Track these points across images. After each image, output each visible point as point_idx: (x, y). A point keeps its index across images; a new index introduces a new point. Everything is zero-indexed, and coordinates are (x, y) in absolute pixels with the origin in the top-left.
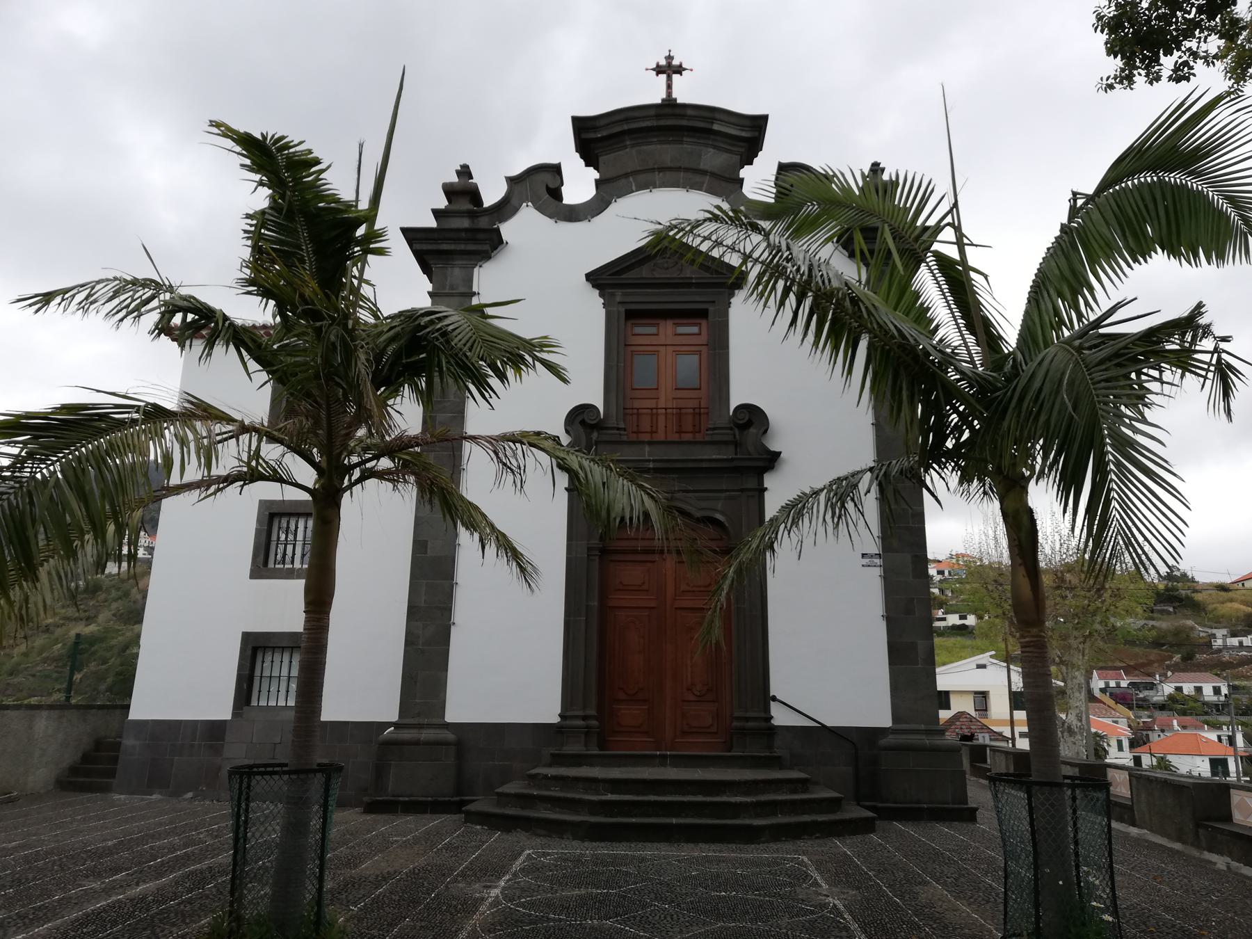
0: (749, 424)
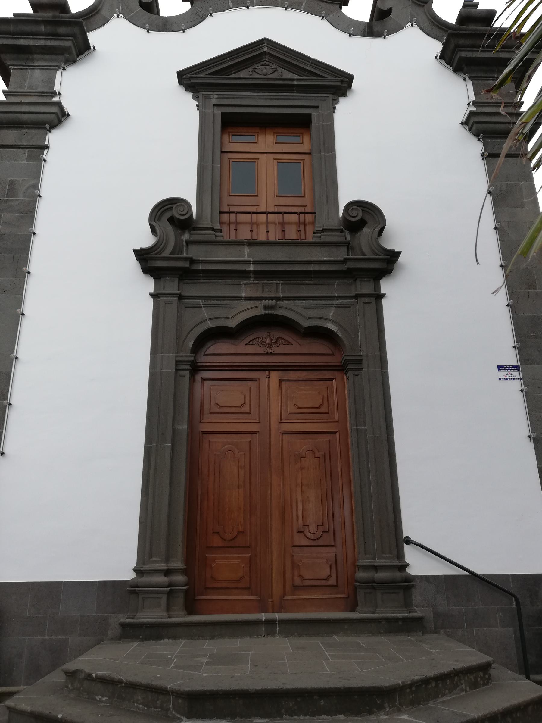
0: (362, 223)
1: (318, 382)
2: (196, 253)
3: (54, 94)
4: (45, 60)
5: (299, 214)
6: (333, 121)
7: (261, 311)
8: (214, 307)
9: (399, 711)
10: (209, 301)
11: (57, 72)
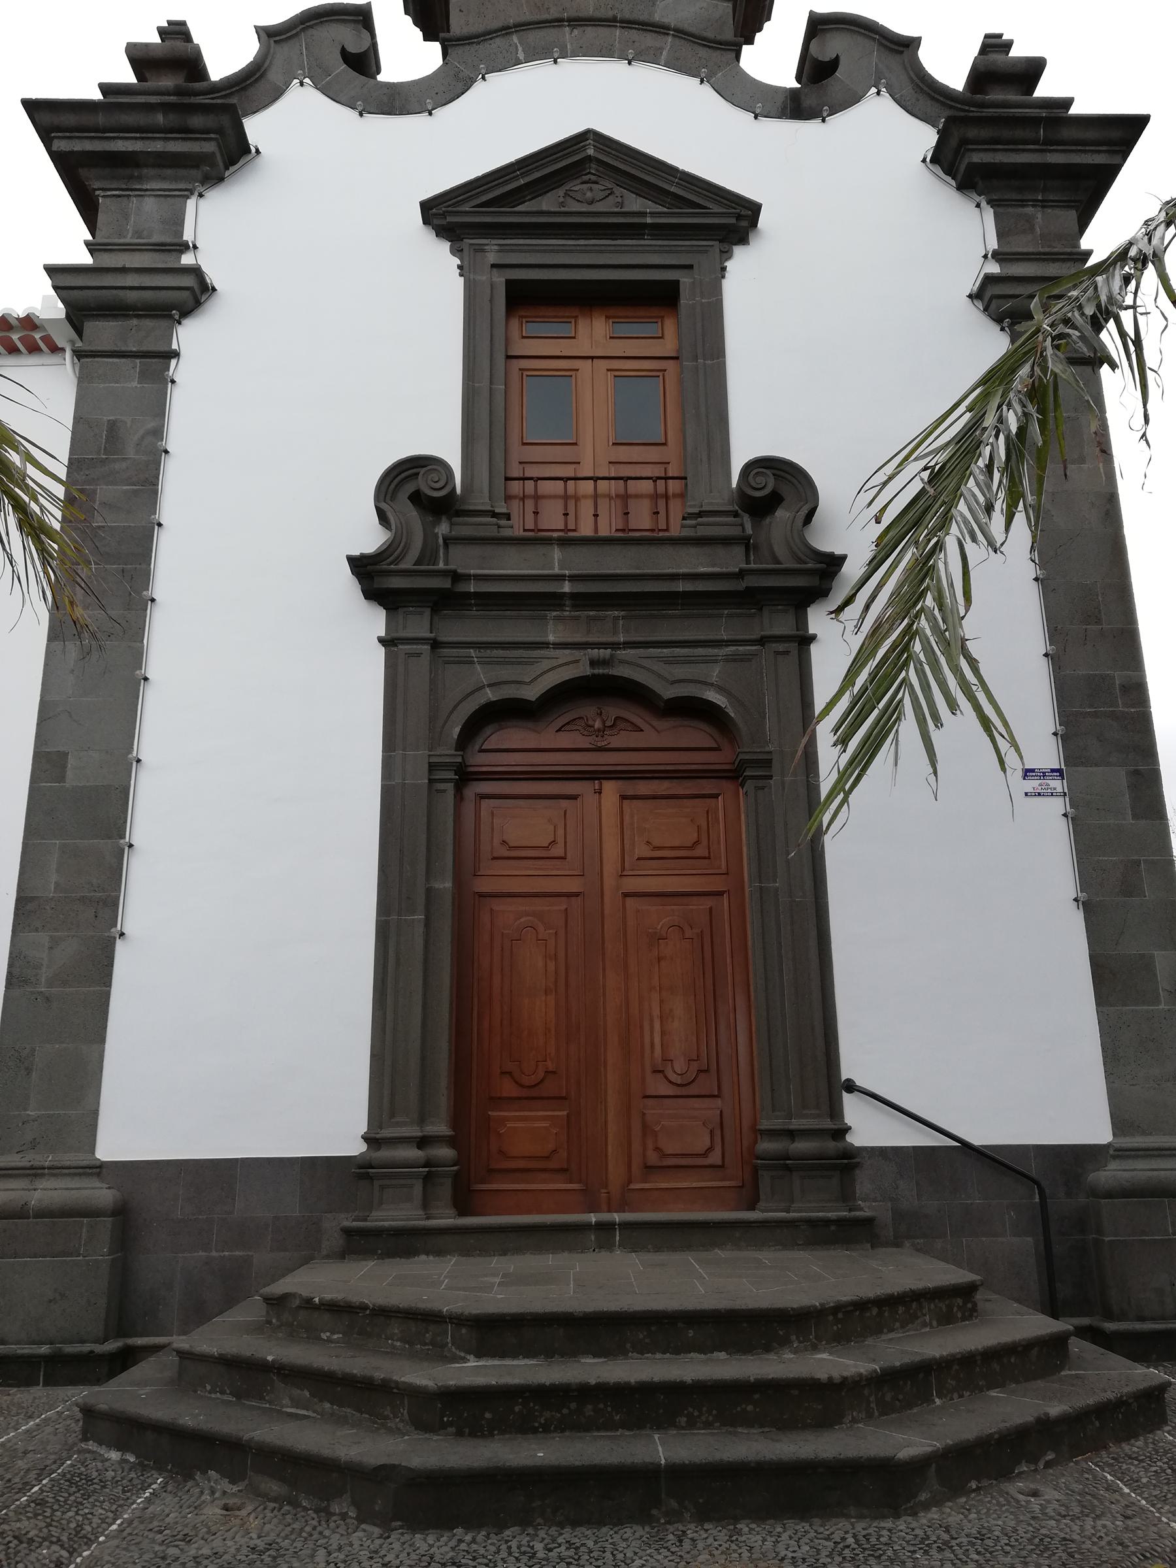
0: (774, 501)
1: (691, 800)
2: (464, 560)
3: (184, 247)
4: (164, 179)
5: (655, 481)
6: (722, 295)
7: (583, 669)
8: (498, 663)
9: (815, 1348)
10: (488, 651)
11: (188, 201)
